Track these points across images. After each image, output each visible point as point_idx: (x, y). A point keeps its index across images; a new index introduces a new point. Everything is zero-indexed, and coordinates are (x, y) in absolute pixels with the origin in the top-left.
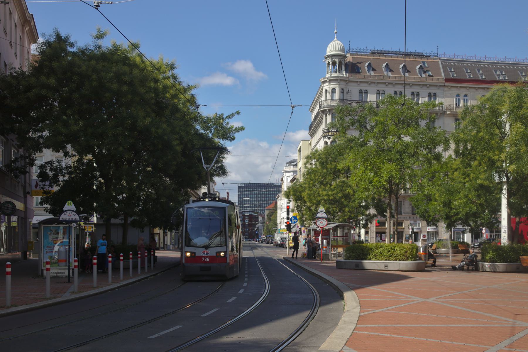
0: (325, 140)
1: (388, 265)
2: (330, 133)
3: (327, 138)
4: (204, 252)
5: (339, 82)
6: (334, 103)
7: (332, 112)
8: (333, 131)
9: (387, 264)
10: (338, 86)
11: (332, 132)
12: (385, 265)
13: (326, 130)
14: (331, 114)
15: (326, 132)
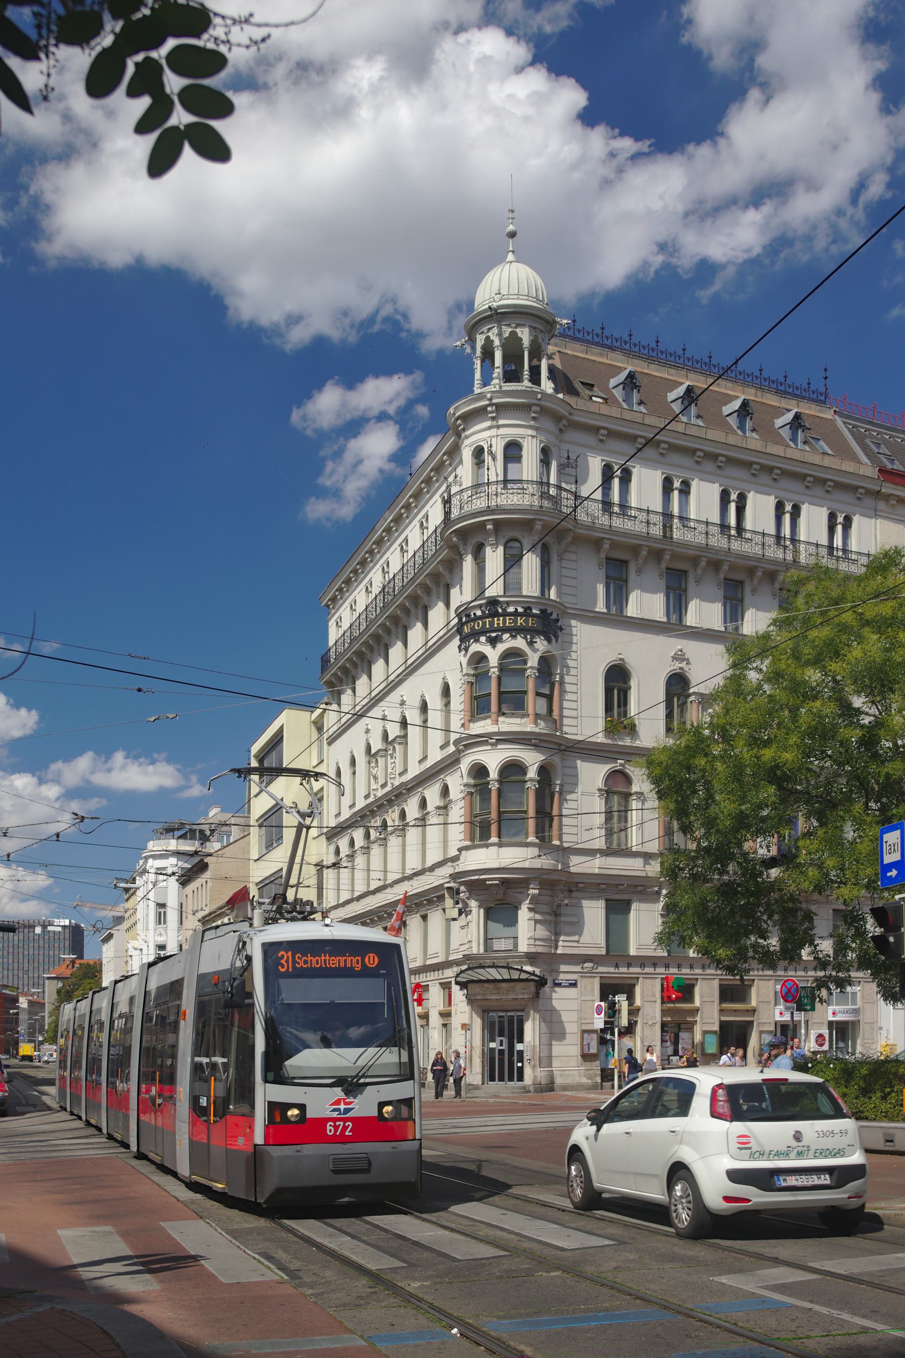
0: (475, 648)
1: (893, 1135)
2: (498, 622)
3: (483, 639)
4: (338, 1102)
5: (534, 419)
6: (512, 499)
7: (520, 538)
8: (511, 609)
9: (891, 1131)
10: (530, 432)
11: (505, 614)
12: (884, 1135)
13: (480, 606)
14: (503, 541)
15: (480, 618)
